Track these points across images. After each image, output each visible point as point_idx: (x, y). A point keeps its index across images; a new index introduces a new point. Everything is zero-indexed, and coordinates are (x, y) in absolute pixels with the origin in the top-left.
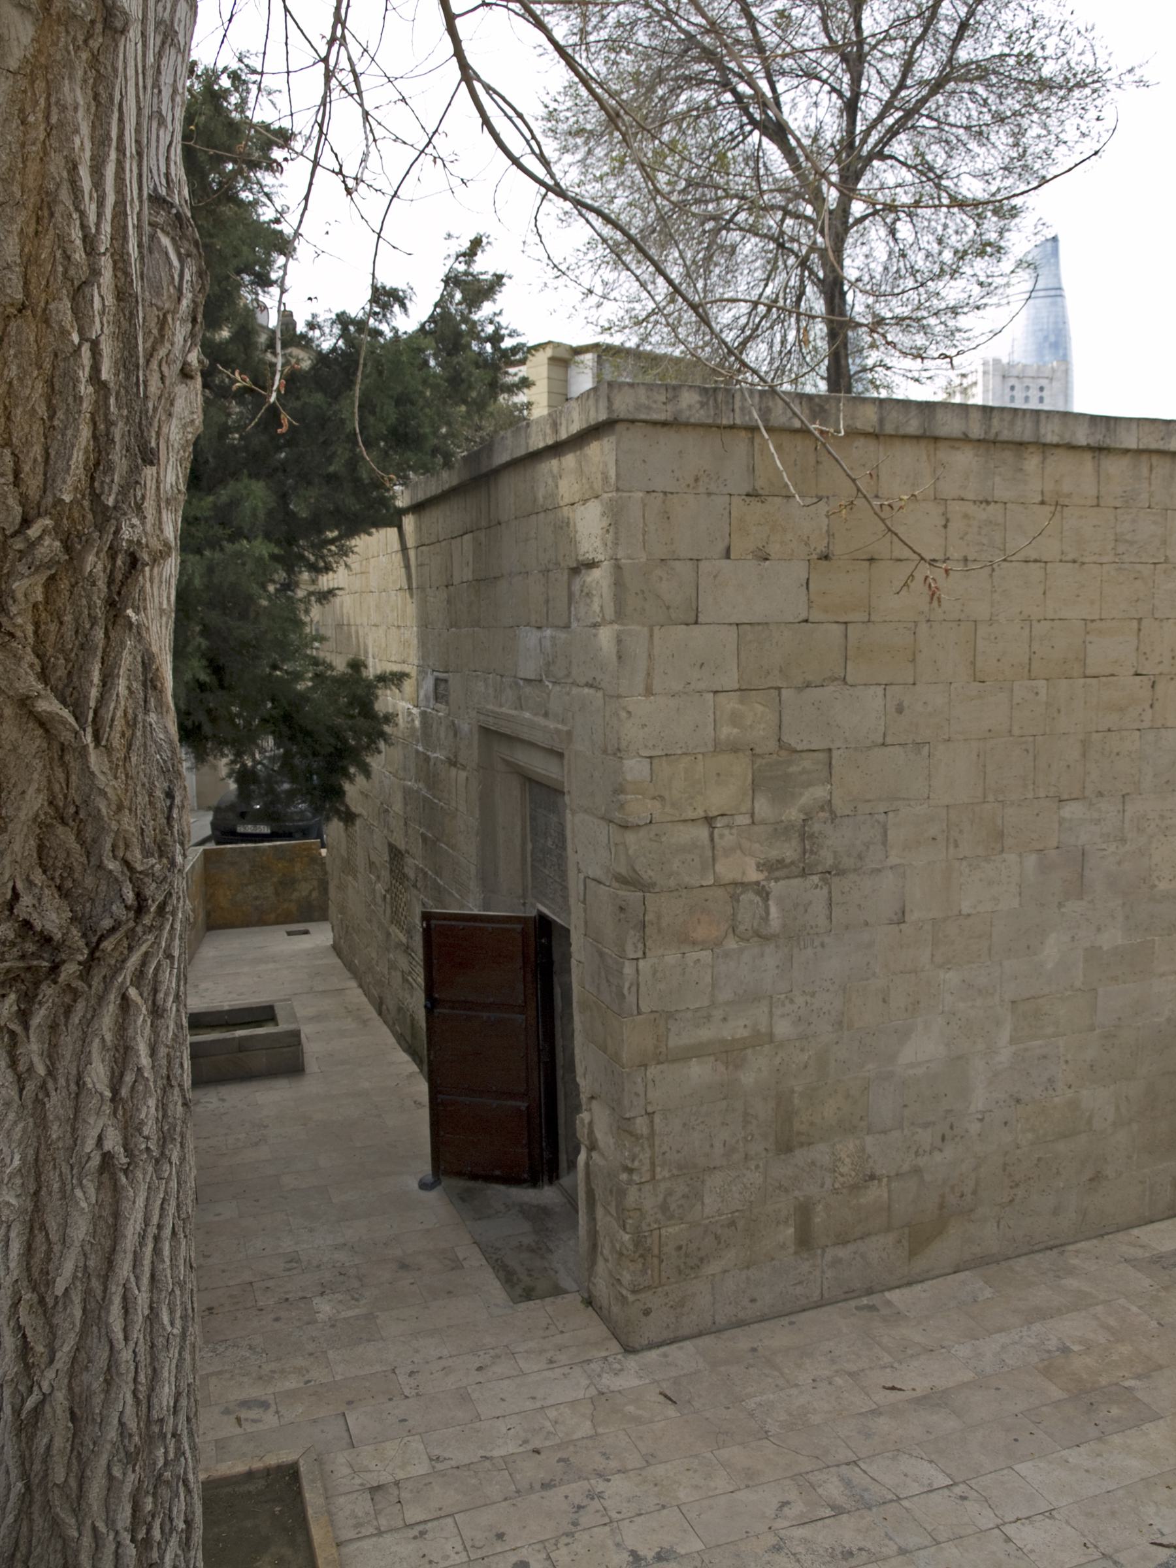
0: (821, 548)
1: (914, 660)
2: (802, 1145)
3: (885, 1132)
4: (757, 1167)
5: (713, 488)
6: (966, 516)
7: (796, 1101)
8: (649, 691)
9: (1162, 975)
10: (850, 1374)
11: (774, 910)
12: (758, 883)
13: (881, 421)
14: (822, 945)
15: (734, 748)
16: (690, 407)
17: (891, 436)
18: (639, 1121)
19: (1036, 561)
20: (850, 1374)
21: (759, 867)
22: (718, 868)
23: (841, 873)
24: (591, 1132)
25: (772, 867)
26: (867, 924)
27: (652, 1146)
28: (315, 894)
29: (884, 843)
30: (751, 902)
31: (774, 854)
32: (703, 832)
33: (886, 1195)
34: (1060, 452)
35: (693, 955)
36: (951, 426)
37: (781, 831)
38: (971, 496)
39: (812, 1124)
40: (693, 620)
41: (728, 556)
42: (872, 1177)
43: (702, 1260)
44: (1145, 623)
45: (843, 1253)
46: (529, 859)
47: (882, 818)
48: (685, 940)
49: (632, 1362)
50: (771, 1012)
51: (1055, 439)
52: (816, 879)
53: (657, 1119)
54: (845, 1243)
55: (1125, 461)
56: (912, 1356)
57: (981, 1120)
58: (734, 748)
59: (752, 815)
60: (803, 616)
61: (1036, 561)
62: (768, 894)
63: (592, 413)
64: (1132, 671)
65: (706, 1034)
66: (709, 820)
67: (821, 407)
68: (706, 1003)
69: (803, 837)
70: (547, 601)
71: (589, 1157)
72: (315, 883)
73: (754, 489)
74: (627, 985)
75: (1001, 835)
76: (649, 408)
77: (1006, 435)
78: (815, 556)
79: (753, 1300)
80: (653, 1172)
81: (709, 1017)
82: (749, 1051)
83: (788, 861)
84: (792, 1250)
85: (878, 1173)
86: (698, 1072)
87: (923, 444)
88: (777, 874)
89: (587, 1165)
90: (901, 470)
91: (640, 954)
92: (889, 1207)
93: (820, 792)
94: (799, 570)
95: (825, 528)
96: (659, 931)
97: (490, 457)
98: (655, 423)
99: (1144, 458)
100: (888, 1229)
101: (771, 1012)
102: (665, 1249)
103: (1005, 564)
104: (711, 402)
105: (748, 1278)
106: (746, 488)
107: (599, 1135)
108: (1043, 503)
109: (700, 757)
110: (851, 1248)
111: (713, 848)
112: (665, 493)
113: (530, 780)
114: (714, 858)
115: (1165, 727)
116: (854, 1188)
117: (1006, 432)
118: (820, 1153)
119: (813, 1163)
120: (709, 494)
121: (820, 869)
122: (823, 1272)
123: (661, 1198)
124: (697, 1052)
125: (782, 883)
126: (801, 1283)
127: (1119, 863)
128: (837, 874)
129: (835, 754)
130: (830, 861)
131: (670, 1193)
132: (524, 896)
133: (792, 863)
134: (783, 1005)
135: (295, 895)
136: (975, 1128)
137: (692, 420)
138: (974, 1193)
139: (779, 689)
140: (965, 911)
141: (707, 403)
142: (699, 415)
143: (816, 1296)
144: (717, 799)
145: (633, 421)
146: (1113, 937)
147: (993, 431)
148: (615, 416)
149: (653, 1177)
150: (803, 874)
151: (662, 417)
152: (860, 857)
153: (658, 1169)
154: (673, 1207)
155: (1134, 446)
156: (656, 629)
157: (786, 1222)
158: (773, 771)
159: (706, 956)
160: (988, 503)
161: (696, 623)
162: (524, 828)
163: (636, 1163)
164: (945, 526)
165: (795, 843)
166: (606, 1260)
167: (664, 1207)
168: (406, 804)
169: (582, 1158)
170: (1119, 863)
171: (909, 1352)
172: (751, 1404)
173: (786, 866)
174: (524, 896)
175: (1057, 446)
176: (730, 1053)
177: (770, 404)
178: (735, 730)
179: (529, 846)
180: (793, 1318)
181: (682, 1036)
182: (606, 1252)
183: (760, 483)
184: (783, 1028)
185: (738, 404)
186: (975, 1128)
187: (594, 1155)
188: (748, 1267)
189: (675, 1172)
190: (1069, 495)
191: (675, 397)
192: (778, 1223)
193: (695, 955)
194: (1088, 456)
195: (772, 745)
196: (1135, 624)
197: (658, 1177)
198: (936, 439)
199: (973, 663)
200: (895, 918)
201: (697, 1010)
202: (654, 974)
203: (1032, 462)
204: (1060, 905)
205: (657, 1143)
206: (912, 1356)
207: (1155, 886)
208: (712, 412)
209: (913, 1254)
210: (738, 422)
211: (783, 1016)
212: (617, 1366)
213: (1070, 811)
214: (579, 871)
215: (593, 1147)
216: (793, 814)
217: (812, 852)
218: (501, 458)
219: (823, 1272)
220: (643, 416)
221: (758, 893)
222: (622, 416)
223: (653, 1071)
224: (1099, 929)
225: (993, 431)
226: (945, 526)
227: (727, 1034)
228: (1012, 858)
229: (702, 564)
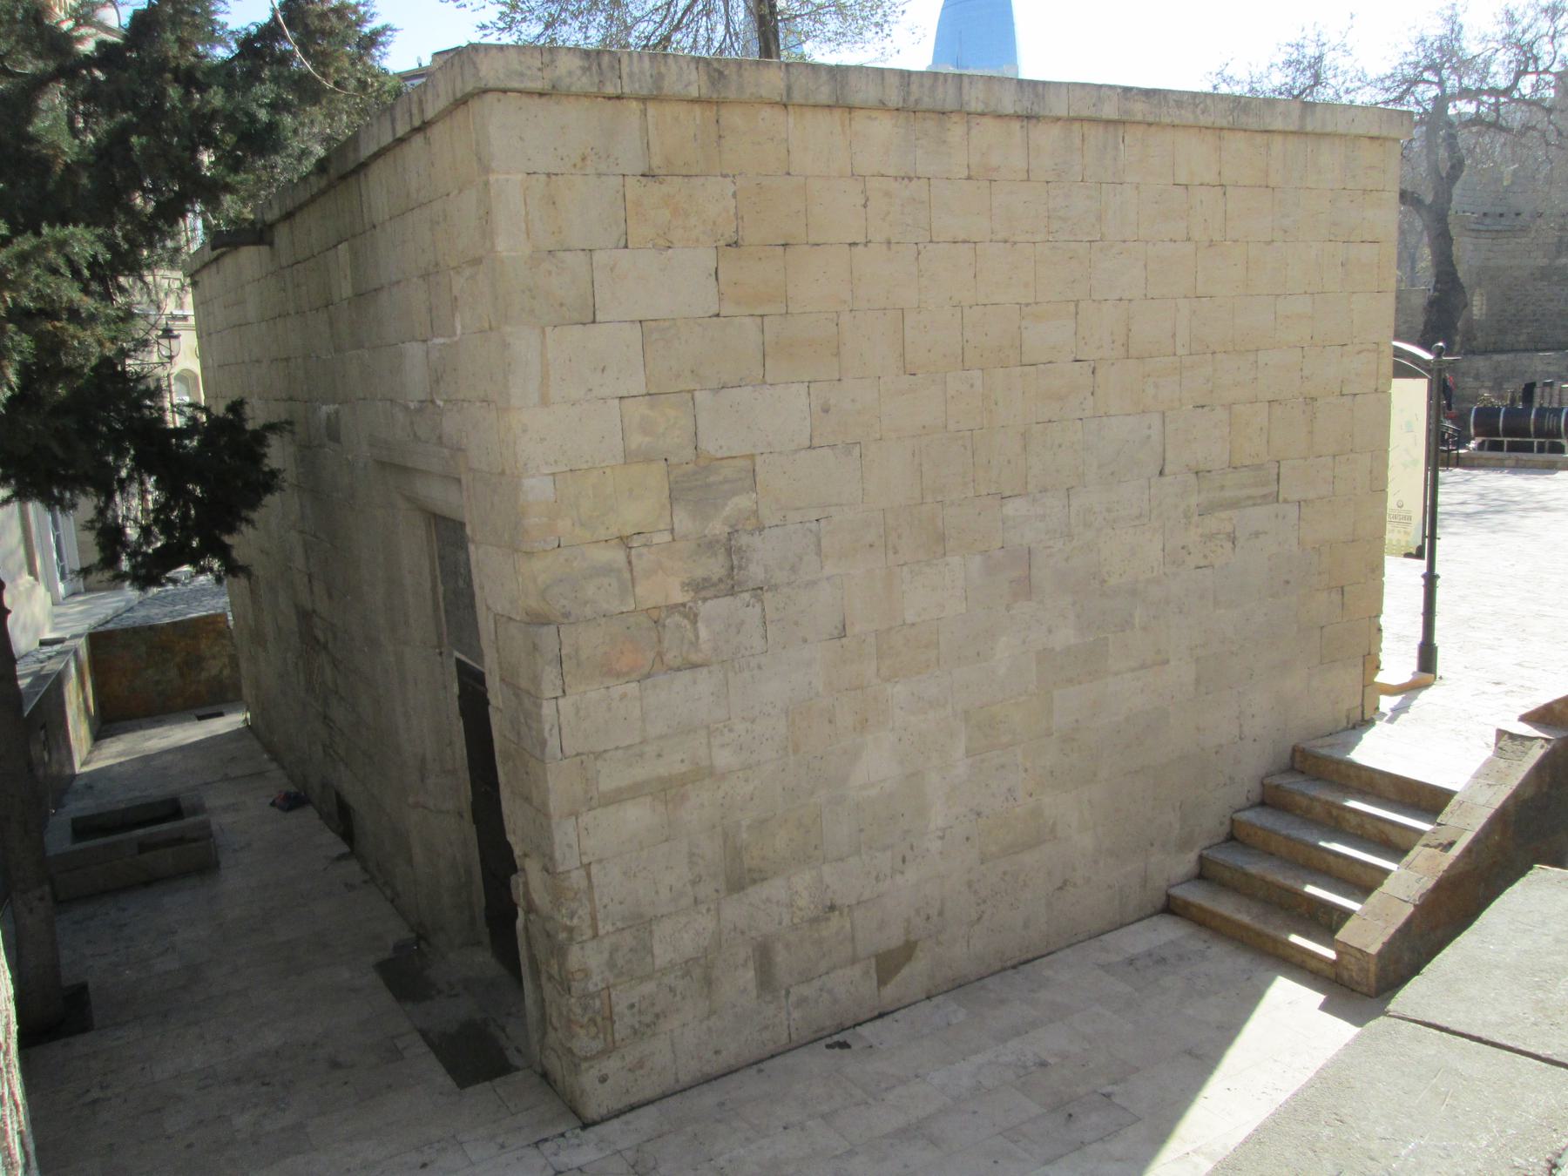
0: (730, 234)
1: (838, 354)
2: (754, 882)
3: (842, 860)
4: (708, 910)
5: (603, 167)
6: (887, 194)
7: (745, 836)
8: (545, 401)
9: (1116, 674)
10: (823, 1117)
11: (704, 633)
12: (684, 605)
13: (789, 89)
14: (759, 667)
15: (647, 458)
16: (570, 73)
17: (801, 105)
18: (575, 874)
19: (964, 242)
20: (823, 1117)
21: (686, 586)
22: (638, 590)
23: (774, 588)
24: (527, 893)
25: (699, 587)
26: (805, 641)
27: (591, 900)
28: (226, 672)
29: (819, 553)
30: (678, 626)
31: (700, 573)
32: (618, 556)
33: (848, 926)
34: (987, 121)
35: (619, 689)
36: (866, 92)
37: (707, 546)
38: (892, 171)
39: (763, 858)
40: (590, 318)
41: (626, 247)
42: (832, 908)
43: (657, 1016)
44: (1082, 305)
45: (806, 990)
46: (442, 604)
47: (814, 526)
48: (610, 672)
49: (592, 1134)
50: (709, 743)
51: (980, 108)
52: (746, 596)
53: (594, 869)
54: (809, 980)
55: (1056, 130)
56: (887, 1089)
57: (942, 838)
58: (647, 458)
59: (672, 530)
60: (715, 310)
61: (964, 242)
62: (696, 615)
63: (459, 84)
64: (1072, 358)
65: (640, 773)
66: (624, 541)
67: (721, 73)
68: (638, 740)
69: (729, 552)
70: (430, 310)
71: (527, 920)
72: (226, 660)
73: (650, 168)
74: (547, 727)
75: (942, 538)
76: (522, 75)
77: (927, 102)
78: (722, 243)
79: (717, 1052)
80: (595, 927)
81: (641, 755)
82: (689, 786)
83: (715, 578)
84: (754, 993)
85: (838, 902)
86: (637, 816)
87: (837, 113)
88: (703, 594)
89: (526, 928)
90: (814, 138)
91: (559, 693)
92: (853, 938)
93: (744, 502)
94: (707, 258)
95: (732, 211)
96: (578, 665)
97: (356, 149)
98: (530, 93)
99: (1077, 125)
100: (854, 961)
101: (709, 743)
102: (616, 1009)
103: (930, 247)
104: (595, 68)
105: (709, 1029)
106: (641, 167)
107: (535, 897)
108: (969, 178)
109: (608, 471)
110: (817, 984)
111: (631, 571)
112: (548, 175)
113: (435, 515)
114: (633, 580)
115: (1107, 415)
116: (815, 920)
117: (926, 99)
118: (774, 889)
119: (768, 900)
120: (599, 175)
121: (751, 585)
122: (789, 1014)
123: (606, 955)
124: (634, 792)
125: (709, 603)
126: (766, 1028)
127: (1067, 560)
128: (769, 589)
129: (759, 460)
130: (761, 576)
131: (614, 950)
132: (440, 646)
133: (721, 580)
134: (722, 734)
135: (204, 675)
136: (936, 846)
137: (573, 89)
138: (941, 914)
139: (692, 392)
140: (909, 619)
141: (589, 68)
142: (583, 83)
143: (784, 1039)
144: (632, 515)
145: (505, 91)
146: (1066, 636)
147: (912, 99)
148: (482, 85)
149: (595, 936)
150: (732, 592)
151: (537, 85)
152: (793, 569)
153: (600, 925)
154: (620, 962)
155: (1063, 113)
156: (548, 330)
157: (745, 965)
158: (693, 483)
159: (633, 688)
160: (910, 179)
161: (594, 322)
162: (433, 570)
163: (576, 921)
164: (865, 206)
165: (722, 558)
166: (555, 1029)
167: (611, 964)
168: (307, 558)
169: (520, 923)
170: (1067, 560)
171: (883, 1085)
172: (721, 1161)
173: (714, 585)
174: (440, 646)
175: (983, 114)
176: (668, 791)
177: (663, 69)
178: (647, 439)
179: (441, 589)
180: (761, 1066)
181: (611, 777)
182: (554, 1020)
183: (656, 161)
184: (724, 758)
185: (625, 69)
186: (936, 846)
187: (532, 917)
188: (708, 1018)
189: (620, 925)
190: (997, 169)
191: (553, 61)
192: (736, 968)
193: (621, 689)
194: (1016, 125)
195: (689, 453)
196: (1072, 307)
197: (601, 932)
198: (851, 108)
199: (903, 355)
200: (836, 633)
201: (630, 747)
202: (577, 713)
203: (956, 130)
204: (1008, 608)
205: (596, 896)
206: (887, 1089)
207: (1104, 581)
208: (596, 80)
209: (882, 982)
210: (627, 90)
211: (723, 746)
212: (576, 1141)
213: (1011, 508)
214: (488, 608)
215: (531, 908)
216: (717, 528)
217: (740, 568)
218: (367, 149)
219: (789, 1014)
220: (516, 85)
221: (686, 616)
222: (491, 84)
223: (586, 819)
224: (1050, 631)
225: (912, 99)
226: (865, 206)
227: (662, 770)
228: (955, 560)
229: (597, 256)
